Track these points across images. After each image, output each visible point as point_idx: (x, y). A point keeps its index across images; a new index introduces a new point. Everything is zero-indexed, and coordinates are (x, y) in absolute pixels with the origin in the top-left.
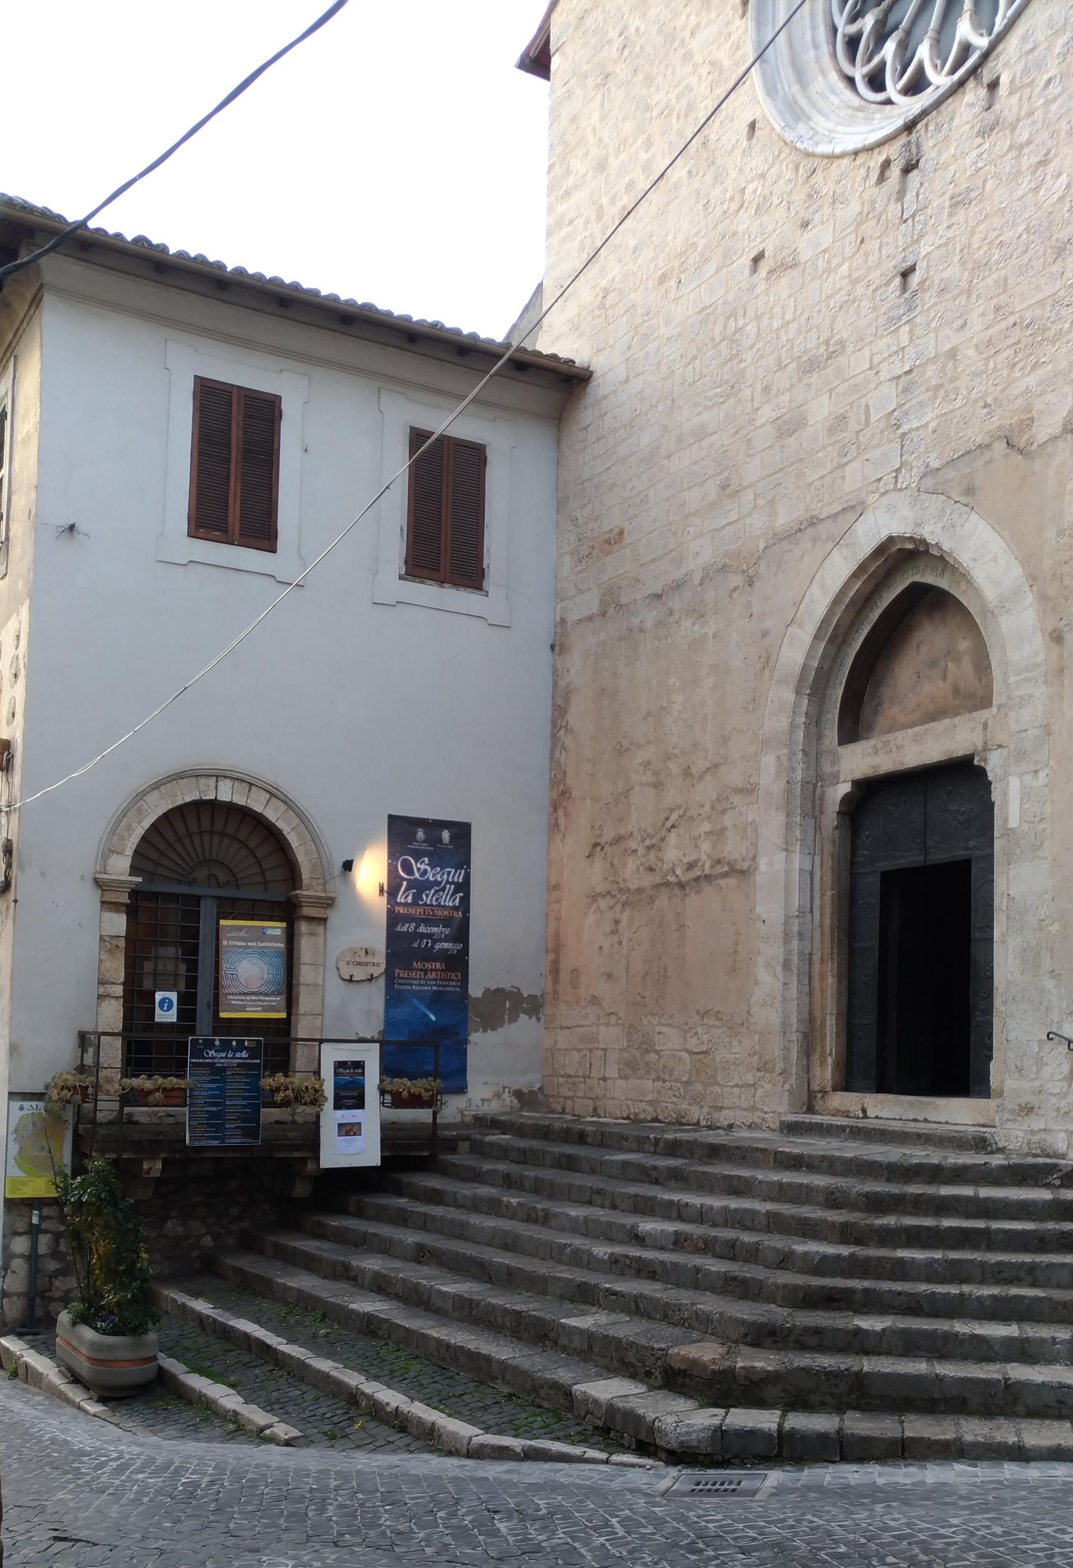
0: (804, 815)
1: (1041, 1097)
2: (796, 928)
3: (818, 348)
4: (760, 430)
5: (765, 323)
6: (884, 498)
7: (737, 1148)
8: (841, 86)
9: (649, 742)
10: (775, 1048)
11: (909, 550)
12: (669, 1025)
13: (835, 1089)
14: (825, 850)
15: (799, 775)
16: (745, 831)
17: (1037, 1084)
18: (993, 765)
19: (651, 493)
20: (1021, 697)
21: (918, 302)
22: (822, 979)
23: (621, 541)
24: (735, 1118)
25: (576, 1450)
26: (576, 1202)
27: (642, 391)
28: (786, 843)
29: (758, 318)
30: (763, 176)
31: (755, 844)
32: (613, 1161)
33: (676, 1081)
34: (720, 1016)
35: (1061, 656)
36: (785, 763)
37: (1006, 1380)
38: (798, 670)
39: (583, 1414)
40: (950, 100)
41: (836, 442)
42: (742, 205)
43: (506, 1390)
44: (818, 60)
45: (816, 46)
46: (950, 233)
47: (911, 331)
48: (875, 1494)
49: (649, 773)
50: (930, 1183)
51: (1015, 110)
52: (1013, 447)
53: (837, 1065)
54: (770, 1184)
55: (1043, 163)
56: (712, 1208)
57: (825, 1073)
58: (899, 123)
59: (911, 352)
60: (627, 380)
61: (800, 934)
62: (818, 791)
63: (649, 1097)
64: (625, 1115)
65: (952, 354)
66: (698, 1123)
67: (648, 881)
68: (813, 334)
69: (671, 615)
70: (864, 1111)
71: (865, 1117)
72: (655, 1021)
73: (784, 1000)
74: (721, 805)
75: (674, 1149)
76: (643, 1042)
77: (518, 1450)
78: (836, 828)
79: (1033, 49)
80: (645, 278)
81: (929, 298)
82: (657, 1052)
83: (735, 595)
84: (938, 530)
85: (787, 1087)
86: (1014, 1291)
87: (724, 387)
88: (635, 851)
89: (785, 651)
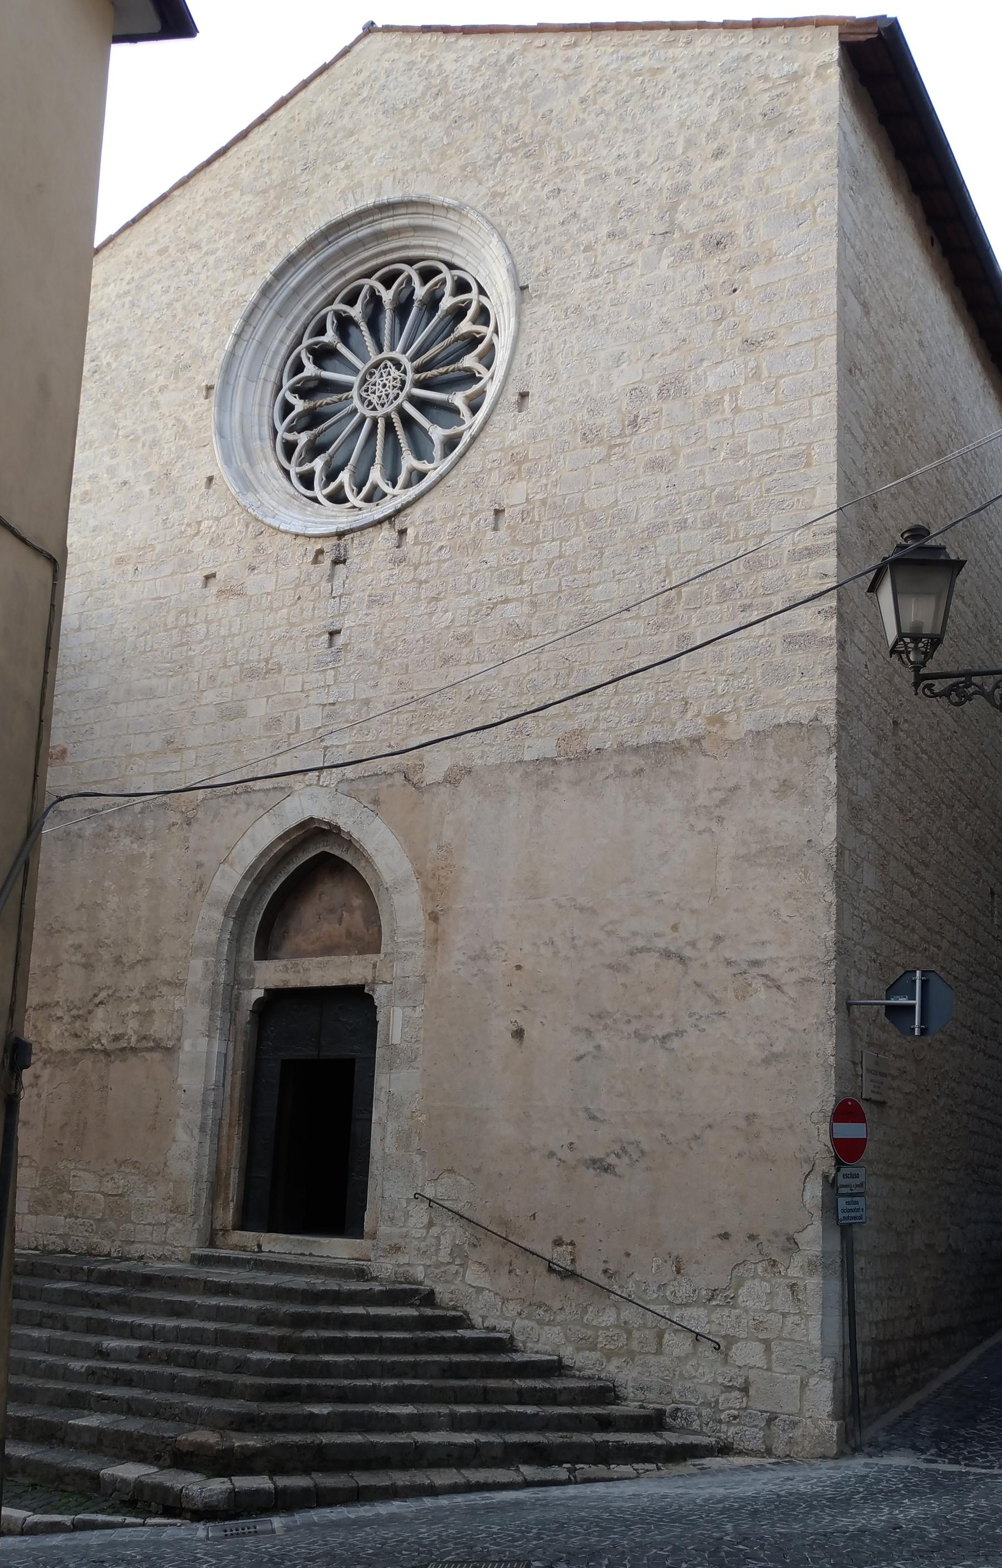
0: (224, 1010)
1: (407, 1240)
2: (212, 1099)
3: (259, 662)
4: (205, 708)
5: (213, 628)
6: (309, 788)
7: (170, 1278)
8: (280, 474)
9: (81, 929)
10: (189, 1195)
11: (324, 829)
12: (85, 1170)
13: (234, 1229)
14: (239, 1038)
15: (222, 979)
16: (172, 1015)
17: (405, 1230)
18: (380, 994)
19: (97, 727)
20: (406, 953)
21: (342, 657)
22: (230, 1138)
23: (63, 758)
24: (145, 1251)
25: (119, 1519)
26: (25, 1324)
27: (94, 643)
28: (209, 1031)
29: (208, 622)
30: (217, 519)
31: (181, 1028)
32: (55, 1289)
33: (89, 1218)
34: (137, 1165)
35: (436, 931)
36: (212, 968)
37: (416, 1443)
38: (227, 899)
39: (109, 1492)
40: (371, 529)
41: (270, 737)
42: (198, 533)
43: (27, 1481)
44: (263, 449)
45: (261, 439)
46: (368, 619)
47: (335, 676)
48: (361, 1523)
49: (79, 956)
50: (331, 1304)
51: (417, 556)
52: (409, 780)
53: (236, 1210)
54: (209, 1307)
55: (436, 599)
56: (164, 1327)
57: (228, 1215)
58: (333, 529)
59: (334, 690)
60: (79, 630)
61: (214, 1103)
62: (235, 992)
63: (61, 1231)
64: (33, 1246)
65: (367, 702)
66: (109, 1254)
67: (72, 1045)
68: (256, 650)
69: (110, 831)
70: (259, 1246)
71: (260, 1251)
72: (72, 1166)
73: (199, 1156)
74: (150, 991)
75: (108, 1278)
76: (56, 1183)
77: (69, 1523)
78: (248, 1023)
79: (432, 522)
80: (103, 554)
81: (351, 658)
82: (70, 1192)
83: (173, 829)
84: (350, 823)
85: (196, 1226)
86: (407, 1382)
87: (174, 665)
88: (60, 1018)
89: (216, 881)
